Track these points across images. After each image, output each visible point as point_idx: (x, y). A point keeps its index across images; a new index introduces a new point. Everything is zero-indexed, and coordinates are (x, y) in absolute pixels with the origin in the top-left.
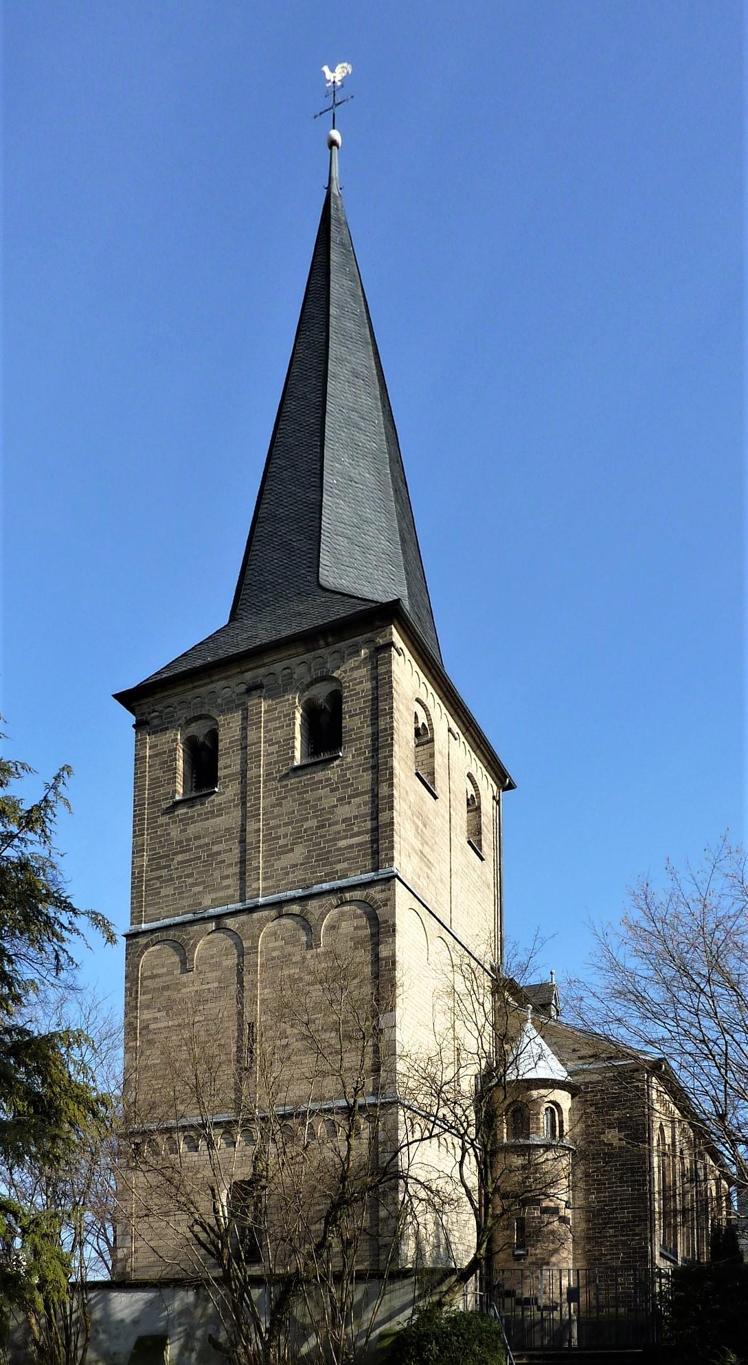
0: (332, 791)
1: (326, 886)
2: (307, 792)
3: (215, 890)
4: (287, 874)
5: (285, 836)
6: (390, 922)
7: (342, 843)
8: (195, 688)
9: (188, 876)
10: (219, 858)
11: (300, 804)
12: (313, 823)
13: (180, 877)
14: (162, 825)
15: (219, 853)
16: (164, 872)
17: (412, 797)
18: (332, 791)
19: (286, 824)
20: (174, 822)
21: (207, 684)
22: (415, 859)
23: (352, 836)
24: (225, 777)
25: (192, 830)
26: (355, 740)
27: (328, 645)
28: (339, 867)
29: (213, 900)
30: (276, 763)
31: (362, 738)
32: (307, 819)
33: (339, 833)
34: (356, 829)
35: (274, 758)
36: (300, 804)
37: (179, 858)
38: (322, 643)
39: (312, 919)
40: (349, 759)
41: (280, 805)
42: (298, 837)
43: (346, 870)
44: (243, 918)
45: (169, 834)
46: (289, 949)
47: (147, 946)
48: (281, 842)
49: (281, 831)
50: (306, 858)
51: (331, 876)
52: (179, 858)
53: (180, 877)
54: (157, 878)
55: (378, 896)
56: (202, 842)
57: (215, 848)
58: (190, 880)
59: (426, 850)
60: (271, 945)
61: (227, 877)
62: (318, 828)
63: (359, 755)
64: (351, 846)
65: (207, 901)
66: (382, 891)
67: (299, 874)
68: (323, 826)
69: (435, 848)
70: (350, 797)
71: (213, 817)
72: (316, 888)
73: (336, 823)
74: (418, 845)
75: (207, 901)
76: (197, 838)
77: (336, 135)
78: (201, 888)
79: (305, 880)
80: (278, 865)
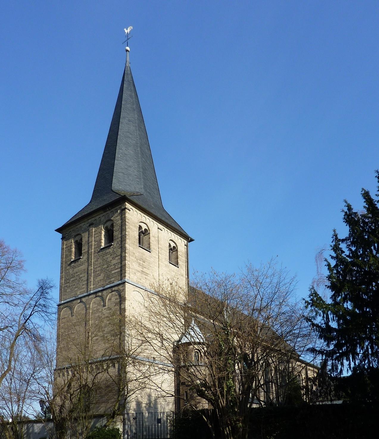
1: (108, 286)
3: (81, 289)
4: (99, 283)
5: (99, 271)
6: (124, 297)
7: (113, 272)
8: (76, 226)
9: (74, 285)
10: (82, 279)
11: (103, 260)
12: (106, 266)
13: (72, 286)
14: (68, 269)
15: (82, 277)
16: (68, 284)
17: (137, 254)
18: (111, 255)
19: (99, 267)
20: (71, 268)
21: (79, 224)
22: (138, 274)
23: (116, 269)
25: (76, 270)
27: (109, 210)
28: (112, 279)
29: (80, 292)
30: (97, 247)
31: (118, 238)
32: (104, 265)
33: (112, 269)
34: (116, 267)
35: (96, 246)
36: (103, 260)
37: (72, 279)
38: (108, 209)
39: (104, 297)
40: (115, 245)
41: (97, 261)
43: (114, 280)
45: (69, 272)
46: (99, 307)
47: (63, 308)
48: (98, 273)
49: (98, 269)
50: (104, 277)
52: (72, 279)
53: (72, 286)
54: (66, 286)
55: (121, 289)
57: (81, 276)
58: (74, 287)
59: (145, 270)
60: (94, 306)
61: (84, 285)
63: (118, 243)
64: (115, 273)
65: (78, 293)
66: (122, 287)
67: (102, 283)
69: (150, 268)
70: (115, 257)
72: (106, 287)
73: (111, 266)
74: (140, 269)
75: (78, 293)
76: (77, 273)
77: (128, 48)
79: (103, 284)
80: (96, 280)
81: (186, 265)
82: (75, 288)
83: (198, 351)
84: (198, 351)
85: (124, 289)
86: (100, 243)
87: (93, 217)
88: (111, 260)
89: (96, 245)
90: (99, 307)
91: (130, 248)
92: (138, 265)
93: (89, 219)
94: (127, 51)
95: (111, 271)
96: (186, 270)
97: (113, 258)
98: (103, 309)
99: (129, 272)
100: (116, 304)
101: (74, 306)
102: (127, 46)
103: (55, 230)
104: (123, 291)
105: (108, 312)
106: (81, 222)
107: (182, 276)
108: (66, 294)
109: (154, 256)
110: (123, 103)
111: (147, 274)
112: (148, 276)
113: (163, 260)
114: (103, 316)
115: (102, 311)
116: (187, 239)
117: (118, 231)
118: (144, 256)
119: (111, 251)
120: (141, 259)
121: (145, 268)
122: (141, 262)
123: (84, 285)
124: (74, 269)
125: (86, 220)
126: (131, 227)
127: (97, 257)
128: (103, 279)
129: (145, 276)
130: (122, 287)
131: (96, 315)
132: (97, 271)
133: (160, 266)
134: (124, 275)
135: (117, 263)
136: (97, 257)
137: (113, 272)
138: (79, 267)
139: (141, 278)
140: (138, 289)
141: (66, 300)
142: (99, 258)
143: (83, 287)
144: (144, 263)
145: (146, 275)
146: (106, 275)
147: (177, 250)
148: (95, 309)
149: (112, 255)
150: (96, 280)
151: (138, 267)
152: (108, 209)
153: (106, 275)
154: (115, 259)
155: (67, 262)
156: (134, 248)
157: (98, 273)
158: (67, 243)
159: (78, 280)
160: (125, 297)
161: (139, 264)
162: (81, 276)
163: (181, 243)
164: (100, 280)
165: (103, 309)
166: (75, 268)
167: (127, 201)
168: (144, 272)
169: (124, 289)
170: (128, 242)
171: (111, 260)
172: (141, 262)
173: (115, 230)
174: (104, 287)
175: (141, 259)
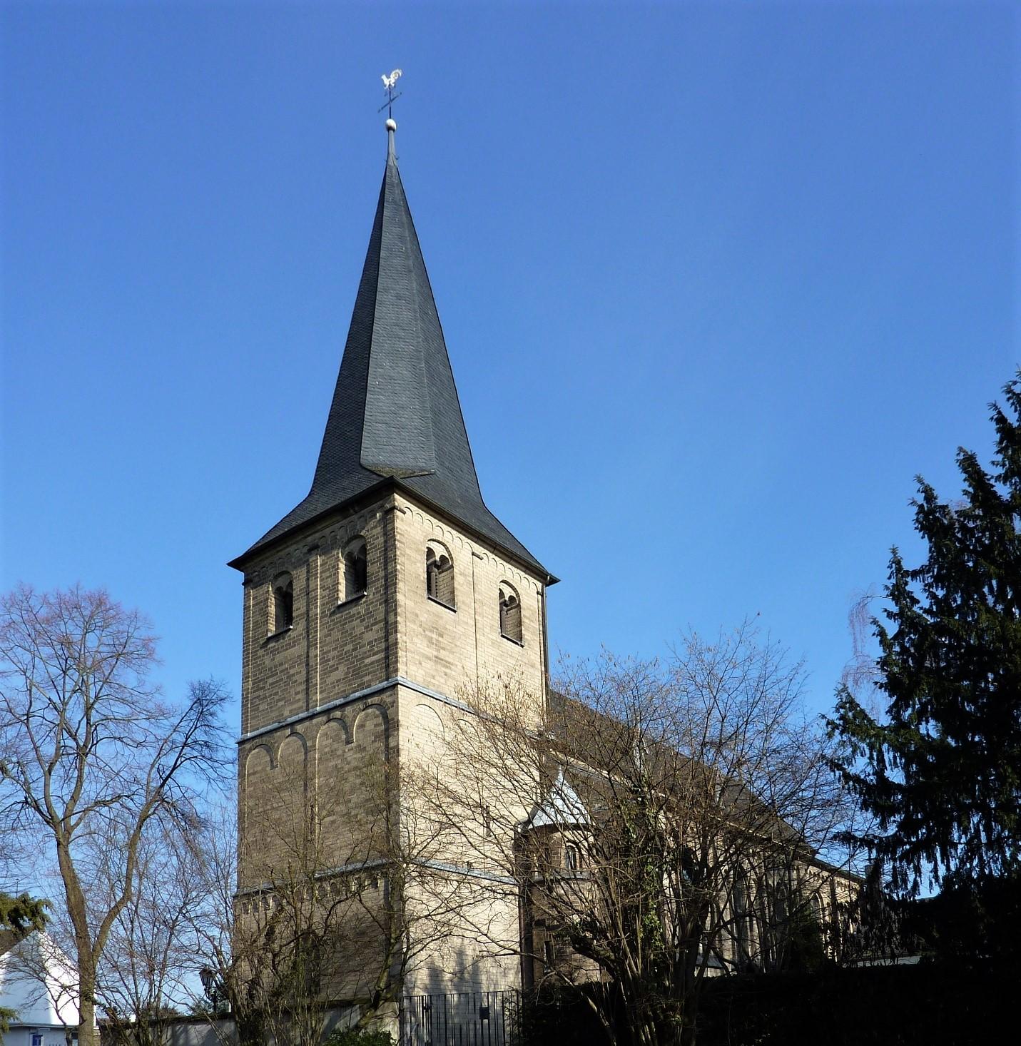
0: (361, 621)
1: (357, 694)
2: (346, 624)
3: (292, 704)
4: (334, 687)
5: (333, 658)
6: (396, 720)
7: (368, 661)
8: (278, 552)
9: (276, 694)
10: (294, 679)
12: (350, 647)
13: (271, 695)
15: (293, 675)
16: (261, 693)
18: (361, 621)
19: (334, 649)
20: (267, 654)
21: (285, 548)
22: (428, 665)
24: (297, 617)
25: (278, 658)
26: (375, 581)
27: (356, 513)
28: (366, 679)
29: (291, 711)
30: (327, 603)
34: (376, 649)
35: (326, 600)
36: (342, 633)
37: (270, 680)
39: (348, 720)
40: (371, 597)
42: (340, 657)
43: (370, 681)
44: (307, 724)
45: (264, 663)
46: (335, 746)
47: (250, 750)
48: (331, 663)
49: (331, 655)
50: (346, 674)
51: (361, 686)
52: (270, 680)
53: (271, 695)
54: (257, 697)
56: (284, 667)
57: (292, 672)
58: (277, 697)
59: (443, 654)
60: (324, 743)
61: (298, 693)
62: (353, 650)
64: (373, 663)
65: (286, 713)
66: (391, 695)
67: (342, 687)
68: (356, 649)
69: (455, 650)
70: (372, 625)
71: (290, 648)
72: (352, 696)
73: (364, 646)
74: (432, 652)
75: (286, 713)
76: (281, 664)
77: (391, 123)
78: (283, 703)
79: (345, 691)
80: (329, 681)
81: (542, 642)
82: (279, 700)
83: (574, 846)
84: (574, 846)
85: (394, 702)
86: (335, 592)
87: (316, 529)
88: (363, 633)
89: (325, 596)
90: (335, 746)
91: (408, 602)
92: (426, 642)
93: (309, 536)
94: (390, 128)
95: (363, 658)
96: (542, 652)
97: (366, 628)
98: (347, 751)
99: (405, 660)
100: (376, 737)
101: (276, 745)
102: (390, 118)
103: (230, 564)
104: (392, 706)
105: (359, 755)
106: (289, 544)
107: (533, 666)
108: (258, 716)
109: (465, 620)
110: (382, 254)
111: (448, 665)
112: (450, 668)
113: (487, 630)
114: (347, 767)
115: (343, 755)
116: (542, 577)
117: (377, 562)
118: (440, 622)
119: (363, 612)
120: (434, 629)
121: (444, 649)
122: (434, 636)
123: (298, 693)
124: (275, 654)
125: (300, 537)
126: (408, 551)
127: (330, 626)
128: (343, 679)
129: (443, 669)
130: (391, 695)
131: (331, 764)
132: (329, 660)
133: (479, 645)
134: (394, 667)
135: (376, 639)
136: (330, 626)
137: (368, 661)
138: (287, 649)
139: (434, 673)
140: (427, 701)
141: (258, 729)
142: (334, 629)
143: (297, 698)
144: (440, 639)
145: (447, 667)
146: (350, 668)
147: (519, 605)
148: (326, 750)
149: (364, 620)
150: (329, 681)
151: (426, 649)
152: (352, 511)
153: (350, 668)
154: (372, 630)
155: (258, 639)
156: (416, 603)
157: (331, 663)
158: (258, 595)
159: (285, 682)
160: (398, 721)
161: (430, 640)
162: (292, 672)
163: (528, 588)
164: (338, 681)
165: (347, 751)
166: (278, 653)
167: (397, 492)
168: (442, 660)
169: (394, 702)
170: (403, 588)
171: (363, 633)
172: (434, 636)
173: (369, 561)
174: (347, 696)
175: (434, 629)
